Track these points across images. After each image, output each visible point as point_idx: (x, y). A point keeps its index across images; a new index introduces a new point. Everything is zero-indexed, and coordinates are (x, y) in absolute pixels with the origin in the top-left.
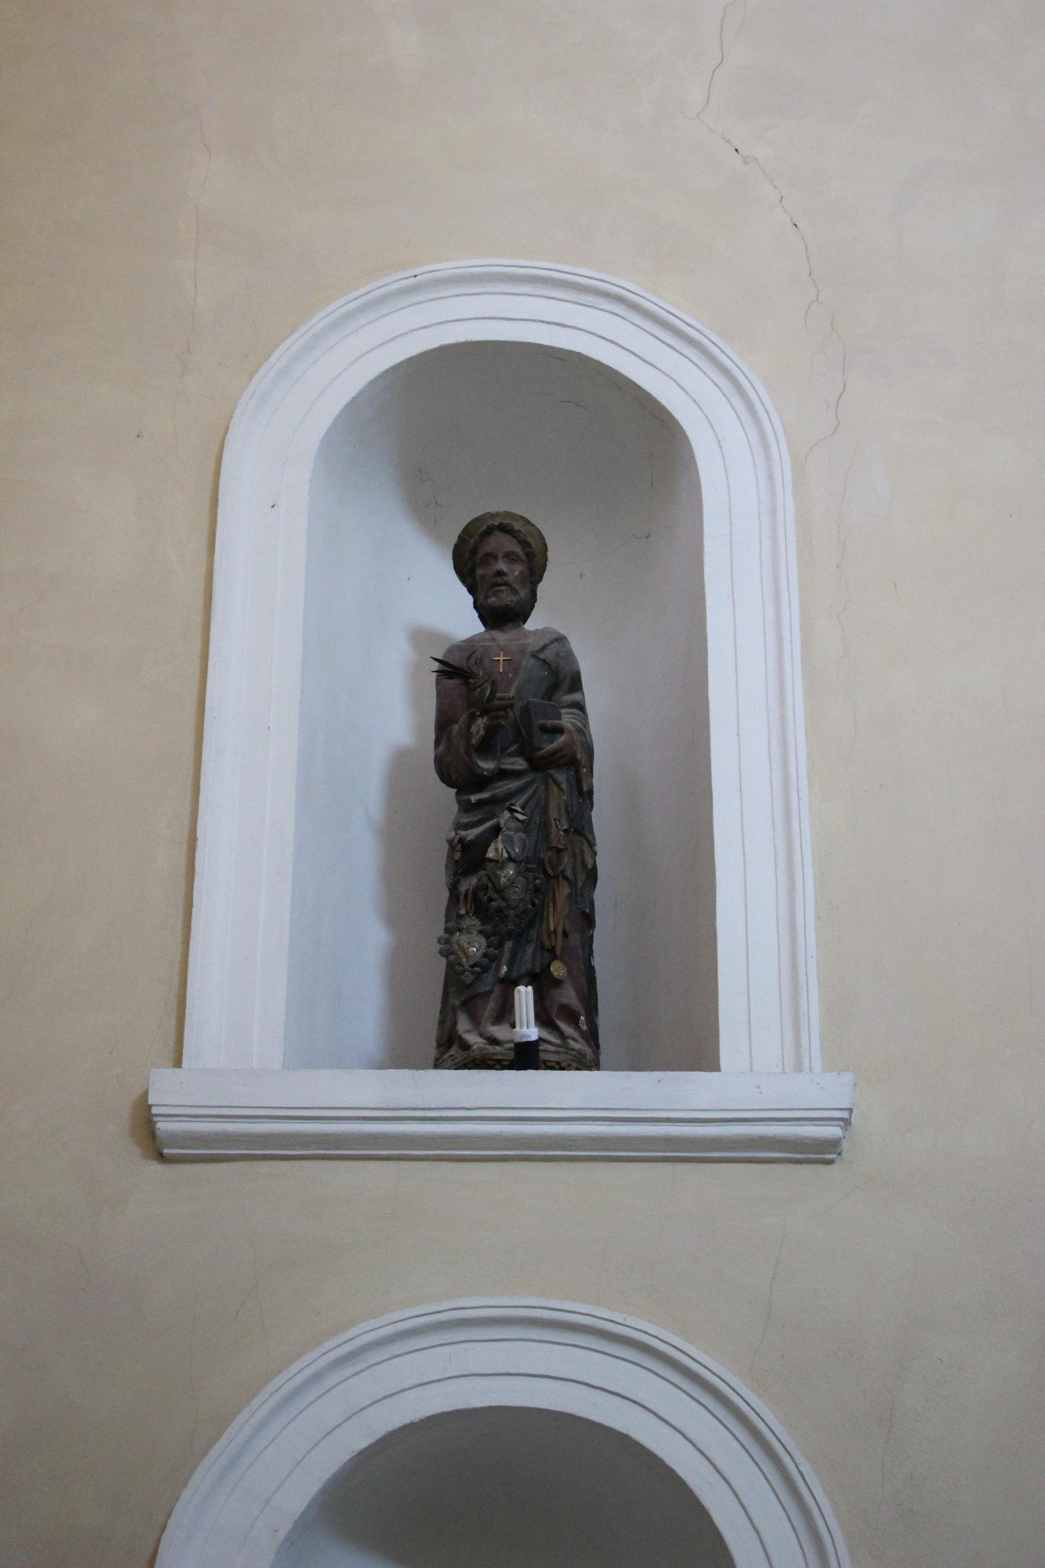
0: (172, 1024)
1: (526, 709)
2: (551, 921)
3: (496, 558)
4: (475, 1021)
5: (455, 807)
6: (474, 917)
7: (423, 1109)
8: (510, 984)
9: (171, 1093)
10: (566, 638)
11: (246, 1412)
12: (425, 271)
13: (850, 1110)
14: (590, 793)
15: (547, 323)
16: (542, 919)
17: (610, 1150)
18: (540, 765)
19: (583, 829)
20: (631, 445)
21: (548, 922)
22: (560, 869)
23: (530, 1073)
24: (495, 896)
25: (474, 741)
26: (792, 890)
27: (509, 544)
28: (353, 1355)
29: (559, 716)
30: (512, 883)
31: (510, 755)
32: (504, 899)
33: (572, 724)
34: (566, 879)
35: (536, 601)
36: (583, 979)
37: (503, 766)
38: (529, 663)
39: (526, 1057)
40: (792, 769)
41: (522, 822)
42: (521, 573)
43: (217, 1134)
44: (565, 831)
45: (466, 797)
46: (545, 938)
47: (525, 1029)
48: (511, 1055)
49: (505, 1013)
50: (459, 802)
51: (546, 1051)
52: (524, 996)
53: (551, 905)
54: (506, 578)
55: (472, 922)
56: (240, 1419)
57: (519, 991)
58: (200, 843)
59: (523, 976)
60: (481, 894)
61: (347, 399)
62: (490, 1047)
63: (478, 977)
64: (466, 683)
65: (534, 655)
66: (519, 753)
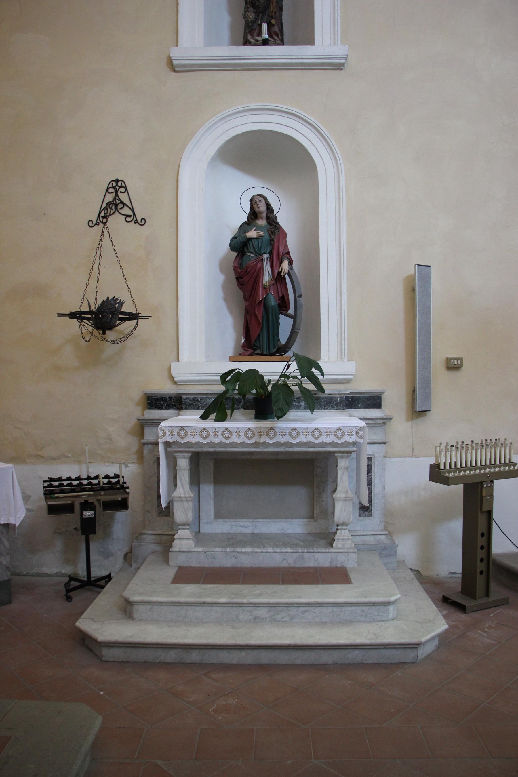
4: (252, 36)
9: (176, 53)
11: (199, 132)
28: (224, 118)
39: (265, 43)
49: (260, 33)
52: (265, 26)
55: (251, 9)
56: (197, 134)
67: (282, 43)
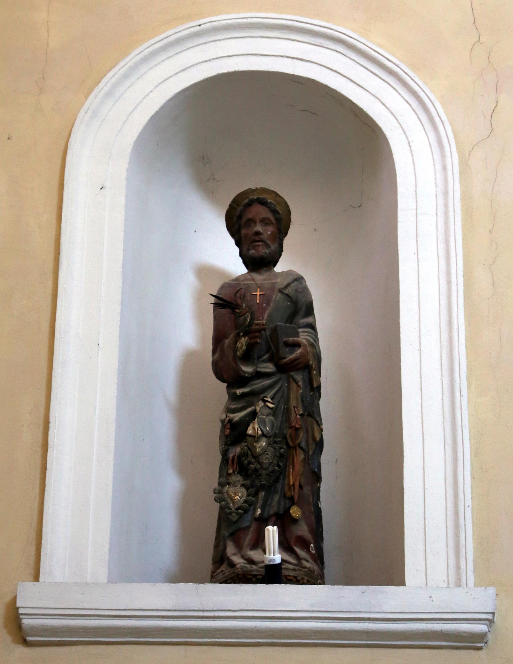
0: (32, 551)
1: (275, 330)
2: (291, 478)
3: (255, 222)
4: (239, 547)
5: (226, 396)
6: (239, 475)
7: (203, 611)
8: (263, 522)
9: (32, 599)
10: (302, 278)
12: (207, 22)
13: (493, 614)
14: (319, 387)
15: (291, 58)
16: (285, 477)
17: (329, 639)
18: (284, 369)
19: (313, 413)
20: (347, 144)
21: (289, 479)
22: (298, 441)
23: (276, 586)
24: (253, 460)
25: (239, 353)
26: (455, 459)
27: (263, 212)
29: (297, 335)
30: (264, 451)
31: (264, 361)
32: (259, 463)
33: (306, 339)
34: (302, 448)
35: (282, 251)
36: (313, 518)
37: (258, 369)
38: (277, 297)
39: (273, 575)
40: (457, 375)
41: (271, 409)
42: (272, 232)
43: (63, 627)
44: (301, 415)
45: (233, 391)
46: (286, 489)
47: (272, 556)
48: (263, 572)
49: (259, 542)
50: (229, 393)
51: (287, 569)
52: (272, 532)
53: (291, 467)
54: (261, 237)
55: (237, 478)
57: (268, 530)
58: (51, 425)
59: (272, 516)
60: (243, 459)
61: (153, 112)
62: (248, 566)
63: (241, 516)
64: (234, 313)
65: (280, 291)
66: (270, 360)
67: (316, 578)
